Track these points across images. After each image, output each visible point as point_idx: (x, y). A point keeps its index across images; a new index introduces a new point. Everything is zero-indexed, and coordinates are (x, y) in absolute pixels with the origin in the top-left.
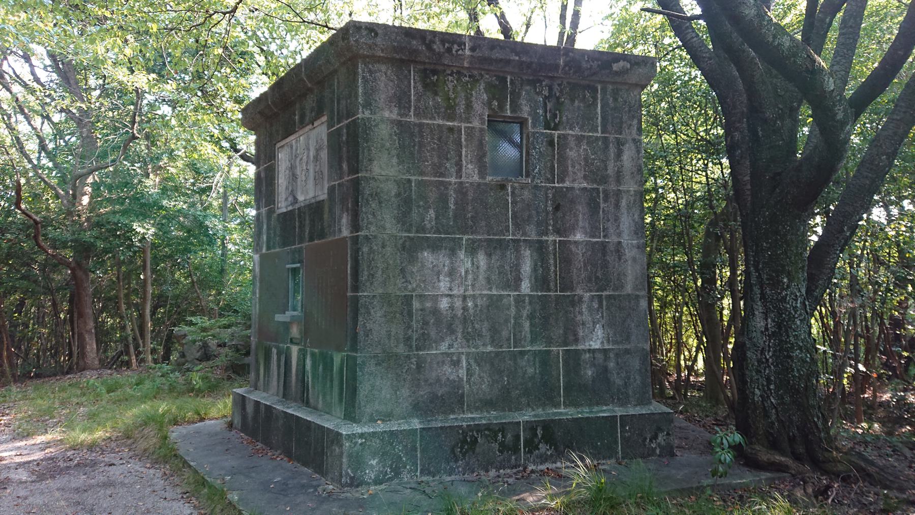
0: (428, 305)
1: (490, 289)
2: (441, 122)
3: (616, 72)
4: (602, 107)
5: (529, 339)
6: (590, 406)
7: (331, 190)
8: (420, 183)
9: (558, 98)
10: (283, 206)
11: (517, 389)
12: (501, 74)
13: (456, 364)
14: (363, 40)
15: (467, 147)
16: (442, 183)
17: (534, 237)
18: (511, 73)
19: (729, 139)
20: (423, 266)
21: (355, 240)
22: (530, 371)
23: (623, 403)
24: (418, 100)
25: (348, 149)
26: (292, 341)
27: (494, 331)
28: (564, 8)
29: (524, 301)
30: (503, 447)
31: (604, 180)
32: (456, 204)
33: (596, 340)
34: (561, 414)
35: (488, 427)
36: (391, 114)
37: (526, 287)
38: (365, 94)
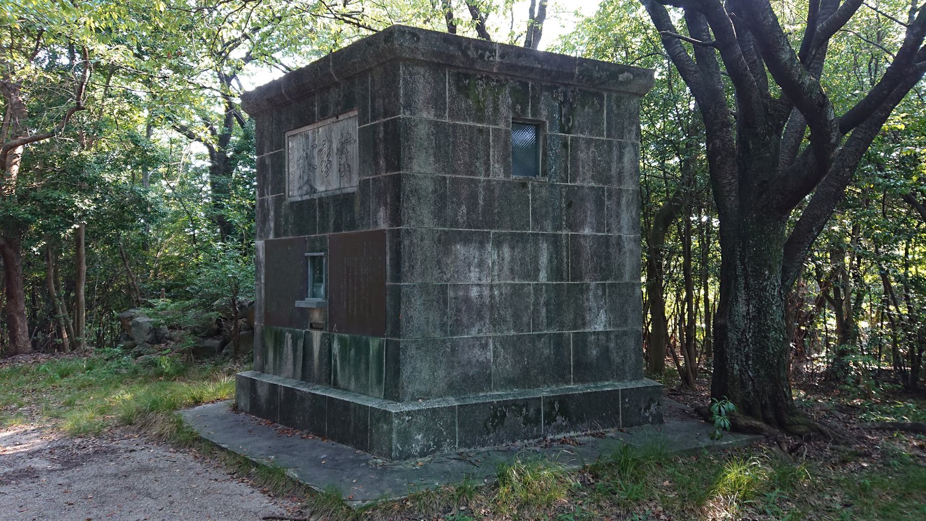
0: (461, 293)
1: (513, 279)
2: (472, 124)
3: (621, 82)
4: (607, 114)
5: (545, 324)
6: (594, 381)
7: (364, 185)
8: (454, 181)
9: (571, 104)
10: (295, 192)
11: (535, 368)
12: (524, 80)
13: (484, 347)
14: (406, 44)
15: (494, 147)
16: (472, 181)
17: (550, 231)
18: (533, 80)
19: (710, 145)
20: (456, 258)
21: (396, 234)
22: (546, 352)
23: (621, 378)
24: (452, 102)
25: (386, 145)
26: (312, 327)
27: (517, 316)
28: (533, 4)
29: (541, 290)
30: (527, 421)
31: (608, 180)
32: (484, 200)
33: (599, 324)
34: (572, 389)
35: (514, 403)
36: (427, 115)
37: (543, 277)
38: (406, 95)
